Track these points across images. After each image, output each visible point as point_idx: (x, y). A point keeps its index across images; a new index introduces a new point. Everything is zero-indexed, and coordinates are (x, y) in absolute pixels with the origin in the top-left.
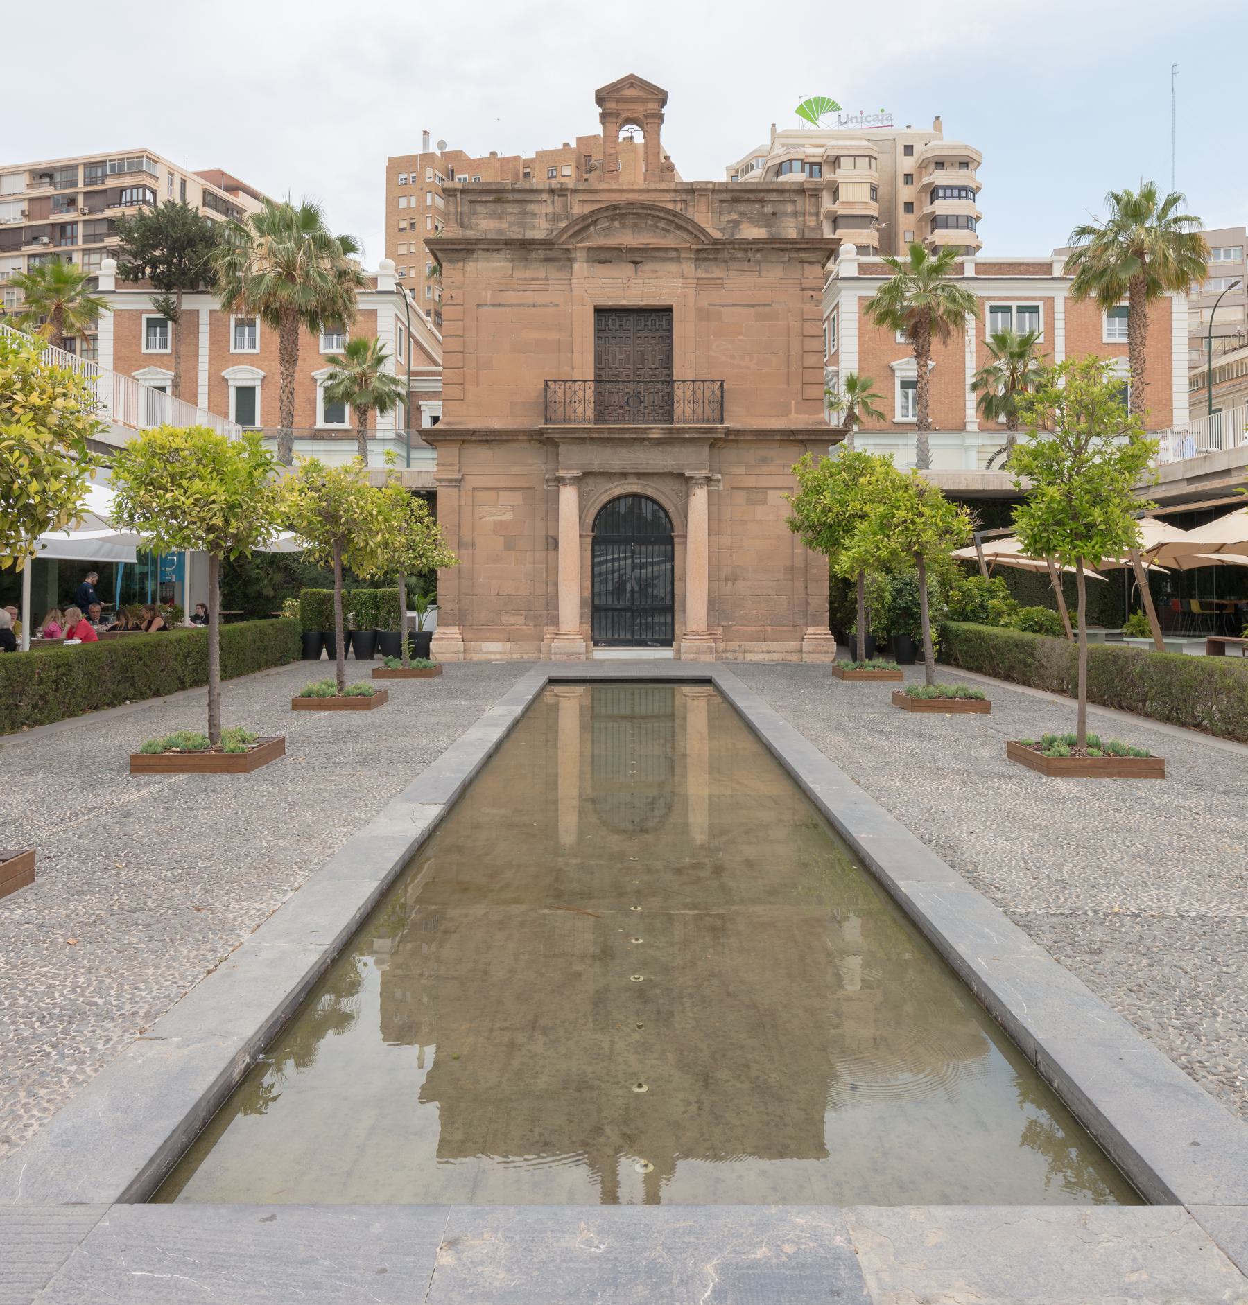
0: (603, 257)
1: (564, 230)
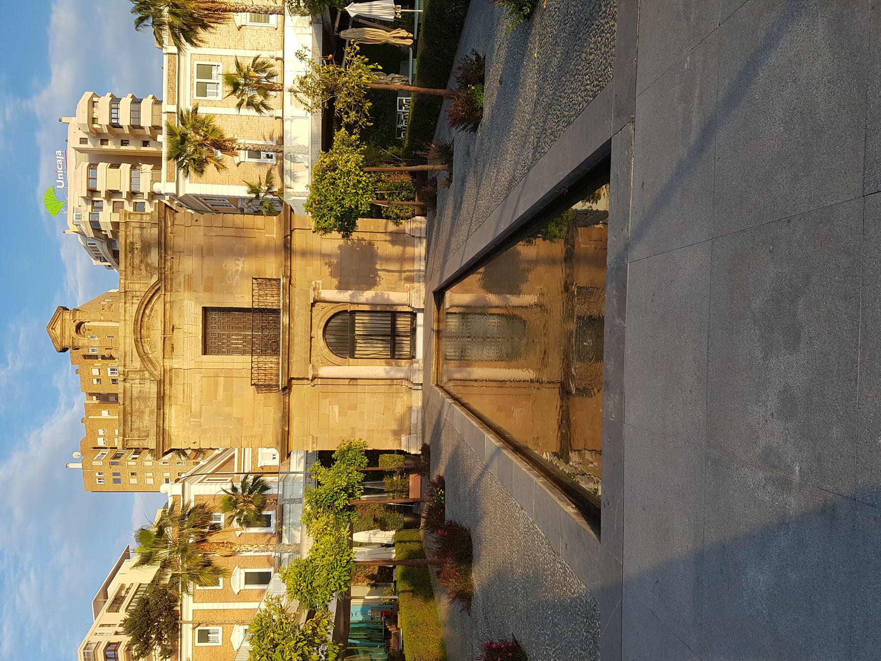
0: (169, 348)
1: (151, 374)
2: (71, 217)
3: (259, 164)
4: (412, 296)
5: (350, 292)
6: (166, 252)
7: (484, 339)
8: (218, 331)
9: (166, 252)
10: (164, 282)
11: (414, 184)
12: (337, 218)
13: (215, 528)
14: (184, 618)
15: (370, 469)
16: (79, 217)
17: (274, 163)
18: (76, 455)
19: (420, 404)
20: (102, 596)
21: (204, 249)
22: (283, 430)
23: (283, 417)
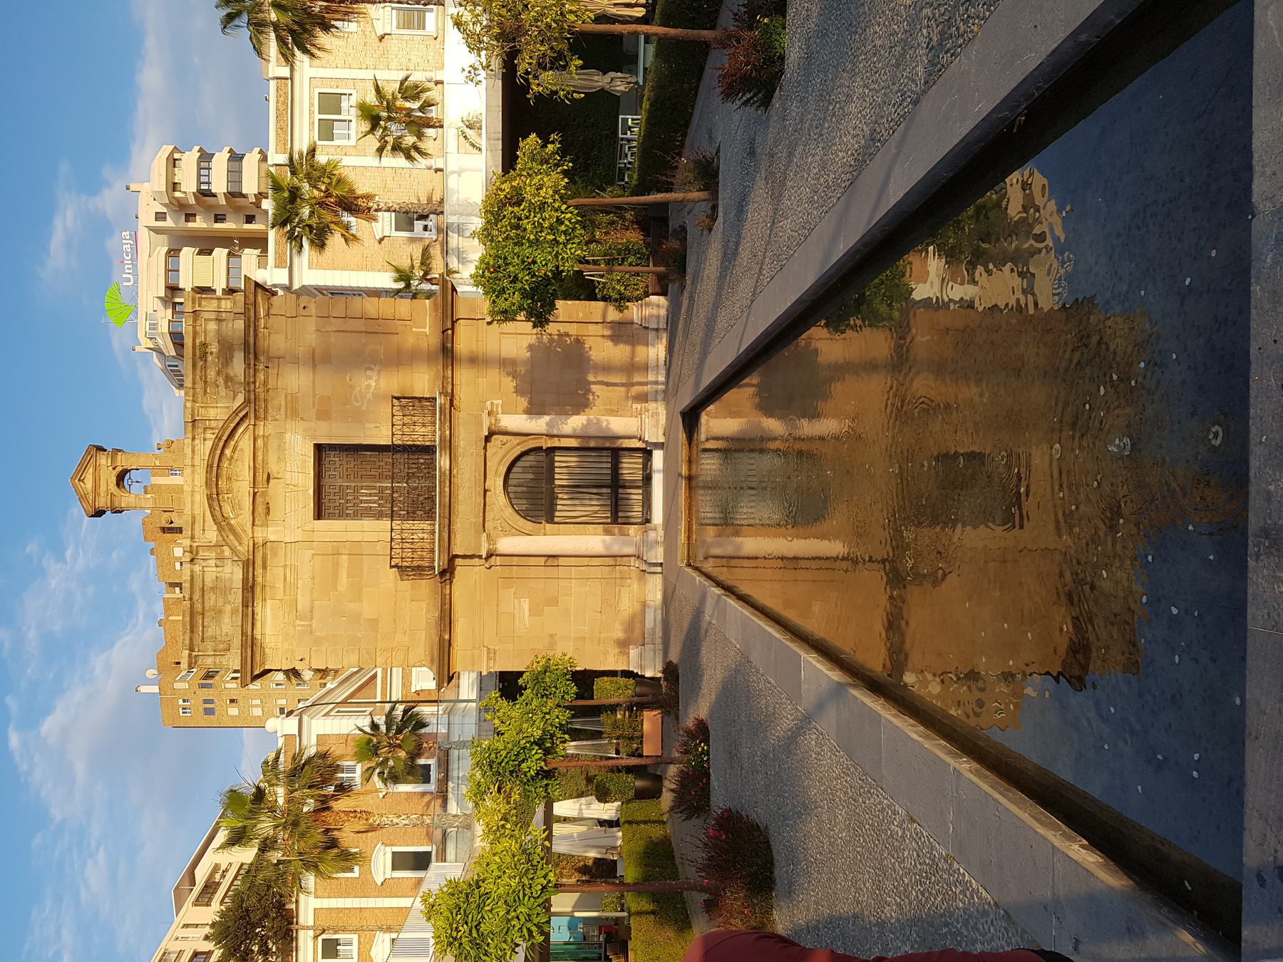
0: (261, 508)
1: (233, 550)
2: (143, 327)
3: (412, 240)
4: (646, 422)
5: (547, 418)
6: (256, 357)
7: (761, 488)
8: (339, 482)
9: (256, 357)
10: (253, 407)
11: (647, 245)
12: (525, 295)
13: (343, 789)
14: (301, 921)
15: (580, 703)
16: (153, 326)
17: (435, 237)
18: (151, 673)
19: (659, 596)
20: (187, 881)
21: (317, 351)
22: (441, 639)
23: (442, 618)
